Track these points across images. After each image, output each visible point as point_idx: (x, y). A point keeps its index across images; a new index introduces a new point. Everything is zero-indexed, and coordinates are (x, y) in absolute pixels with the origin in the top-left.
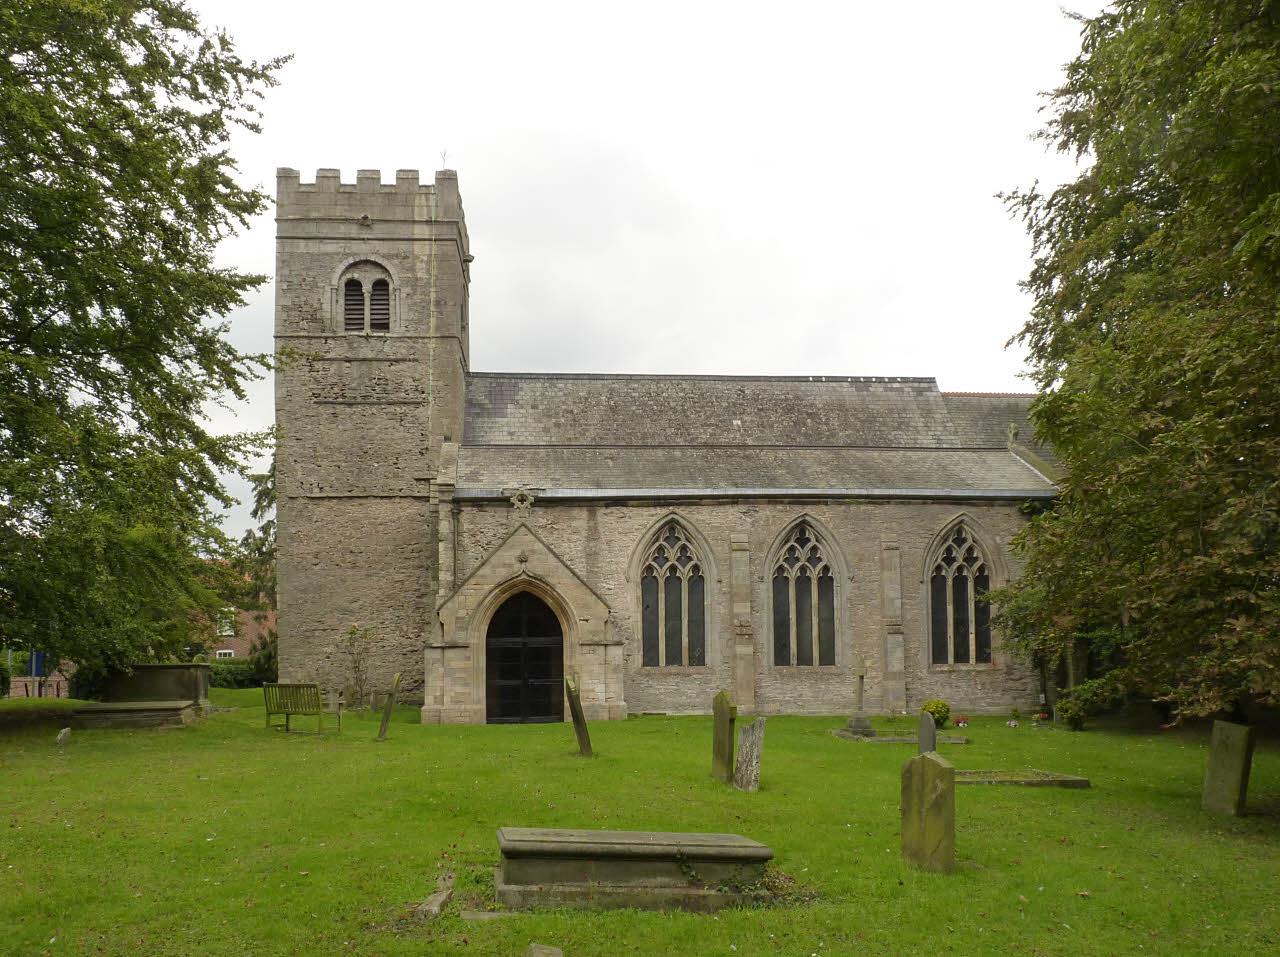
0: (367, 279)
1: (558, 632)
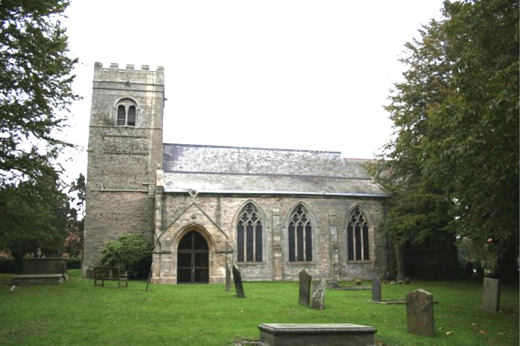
0: (127, 105)
1: (207, 248)
